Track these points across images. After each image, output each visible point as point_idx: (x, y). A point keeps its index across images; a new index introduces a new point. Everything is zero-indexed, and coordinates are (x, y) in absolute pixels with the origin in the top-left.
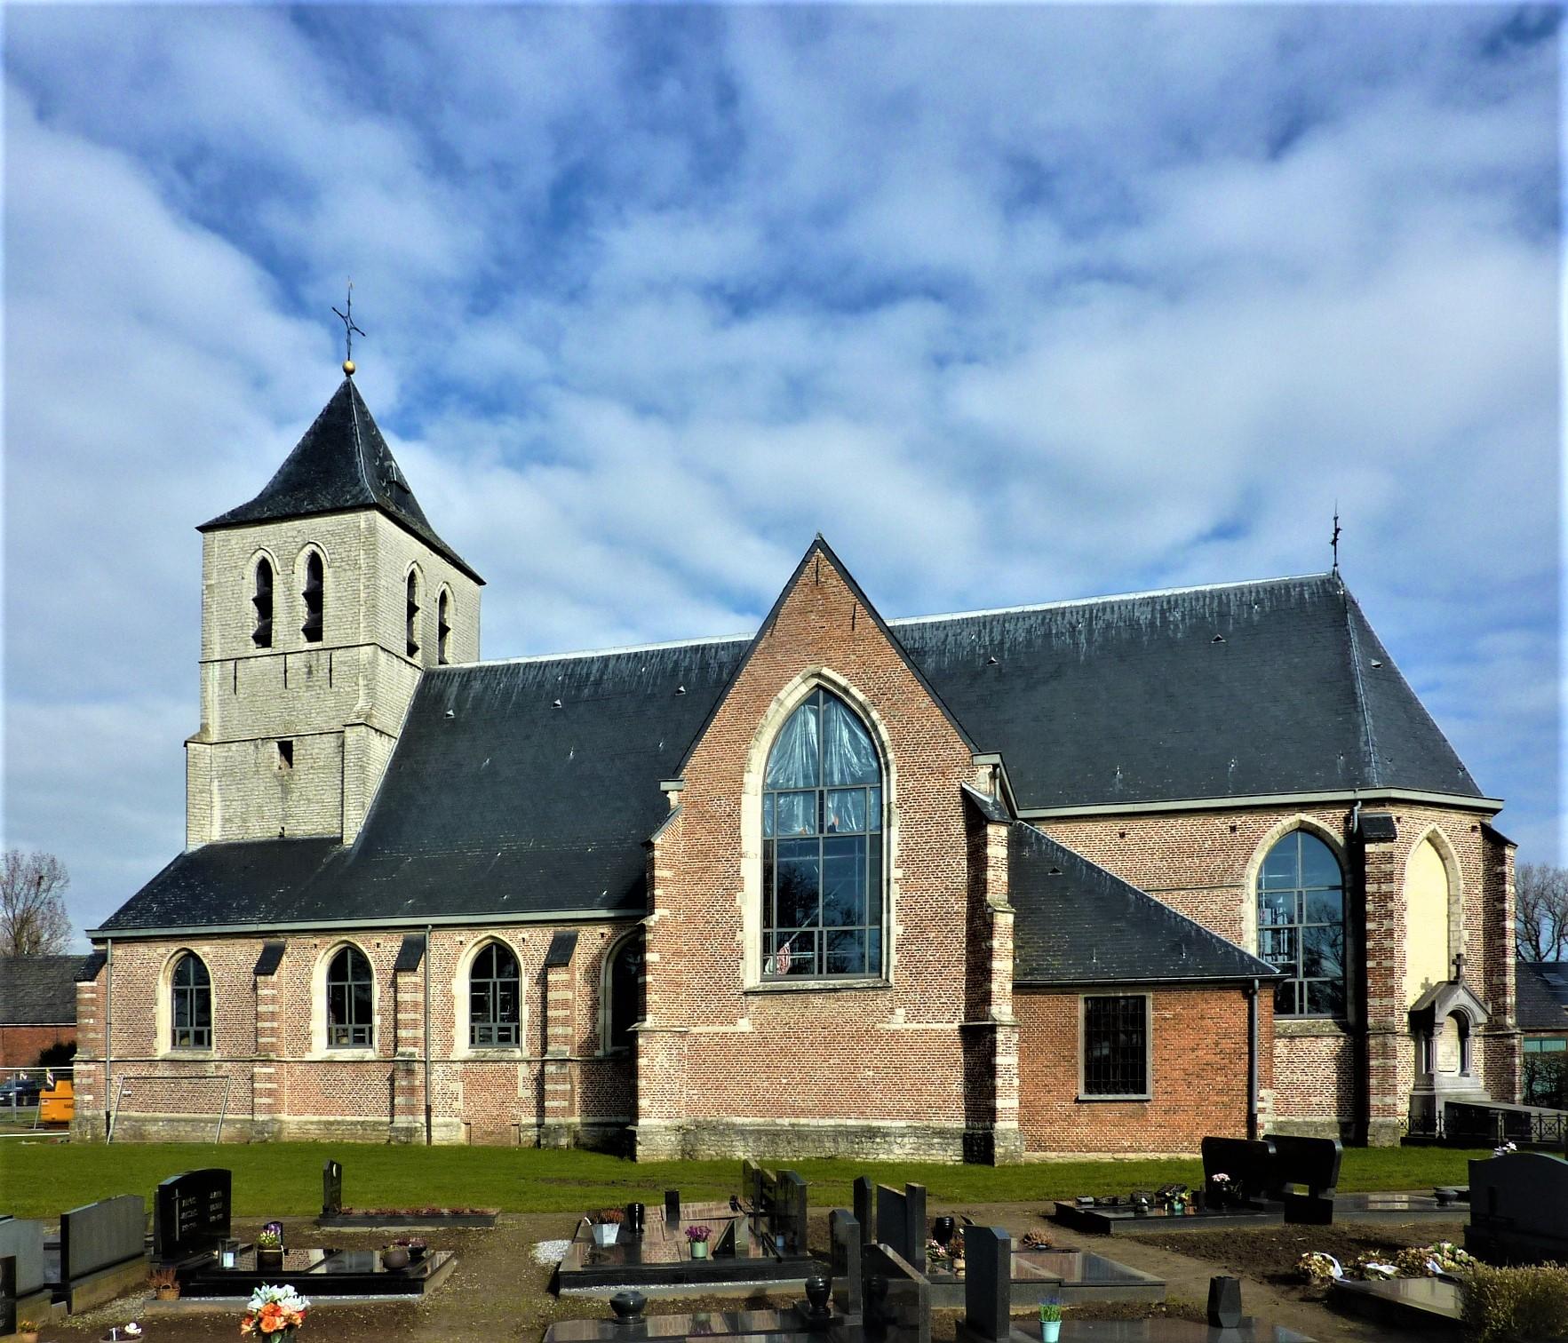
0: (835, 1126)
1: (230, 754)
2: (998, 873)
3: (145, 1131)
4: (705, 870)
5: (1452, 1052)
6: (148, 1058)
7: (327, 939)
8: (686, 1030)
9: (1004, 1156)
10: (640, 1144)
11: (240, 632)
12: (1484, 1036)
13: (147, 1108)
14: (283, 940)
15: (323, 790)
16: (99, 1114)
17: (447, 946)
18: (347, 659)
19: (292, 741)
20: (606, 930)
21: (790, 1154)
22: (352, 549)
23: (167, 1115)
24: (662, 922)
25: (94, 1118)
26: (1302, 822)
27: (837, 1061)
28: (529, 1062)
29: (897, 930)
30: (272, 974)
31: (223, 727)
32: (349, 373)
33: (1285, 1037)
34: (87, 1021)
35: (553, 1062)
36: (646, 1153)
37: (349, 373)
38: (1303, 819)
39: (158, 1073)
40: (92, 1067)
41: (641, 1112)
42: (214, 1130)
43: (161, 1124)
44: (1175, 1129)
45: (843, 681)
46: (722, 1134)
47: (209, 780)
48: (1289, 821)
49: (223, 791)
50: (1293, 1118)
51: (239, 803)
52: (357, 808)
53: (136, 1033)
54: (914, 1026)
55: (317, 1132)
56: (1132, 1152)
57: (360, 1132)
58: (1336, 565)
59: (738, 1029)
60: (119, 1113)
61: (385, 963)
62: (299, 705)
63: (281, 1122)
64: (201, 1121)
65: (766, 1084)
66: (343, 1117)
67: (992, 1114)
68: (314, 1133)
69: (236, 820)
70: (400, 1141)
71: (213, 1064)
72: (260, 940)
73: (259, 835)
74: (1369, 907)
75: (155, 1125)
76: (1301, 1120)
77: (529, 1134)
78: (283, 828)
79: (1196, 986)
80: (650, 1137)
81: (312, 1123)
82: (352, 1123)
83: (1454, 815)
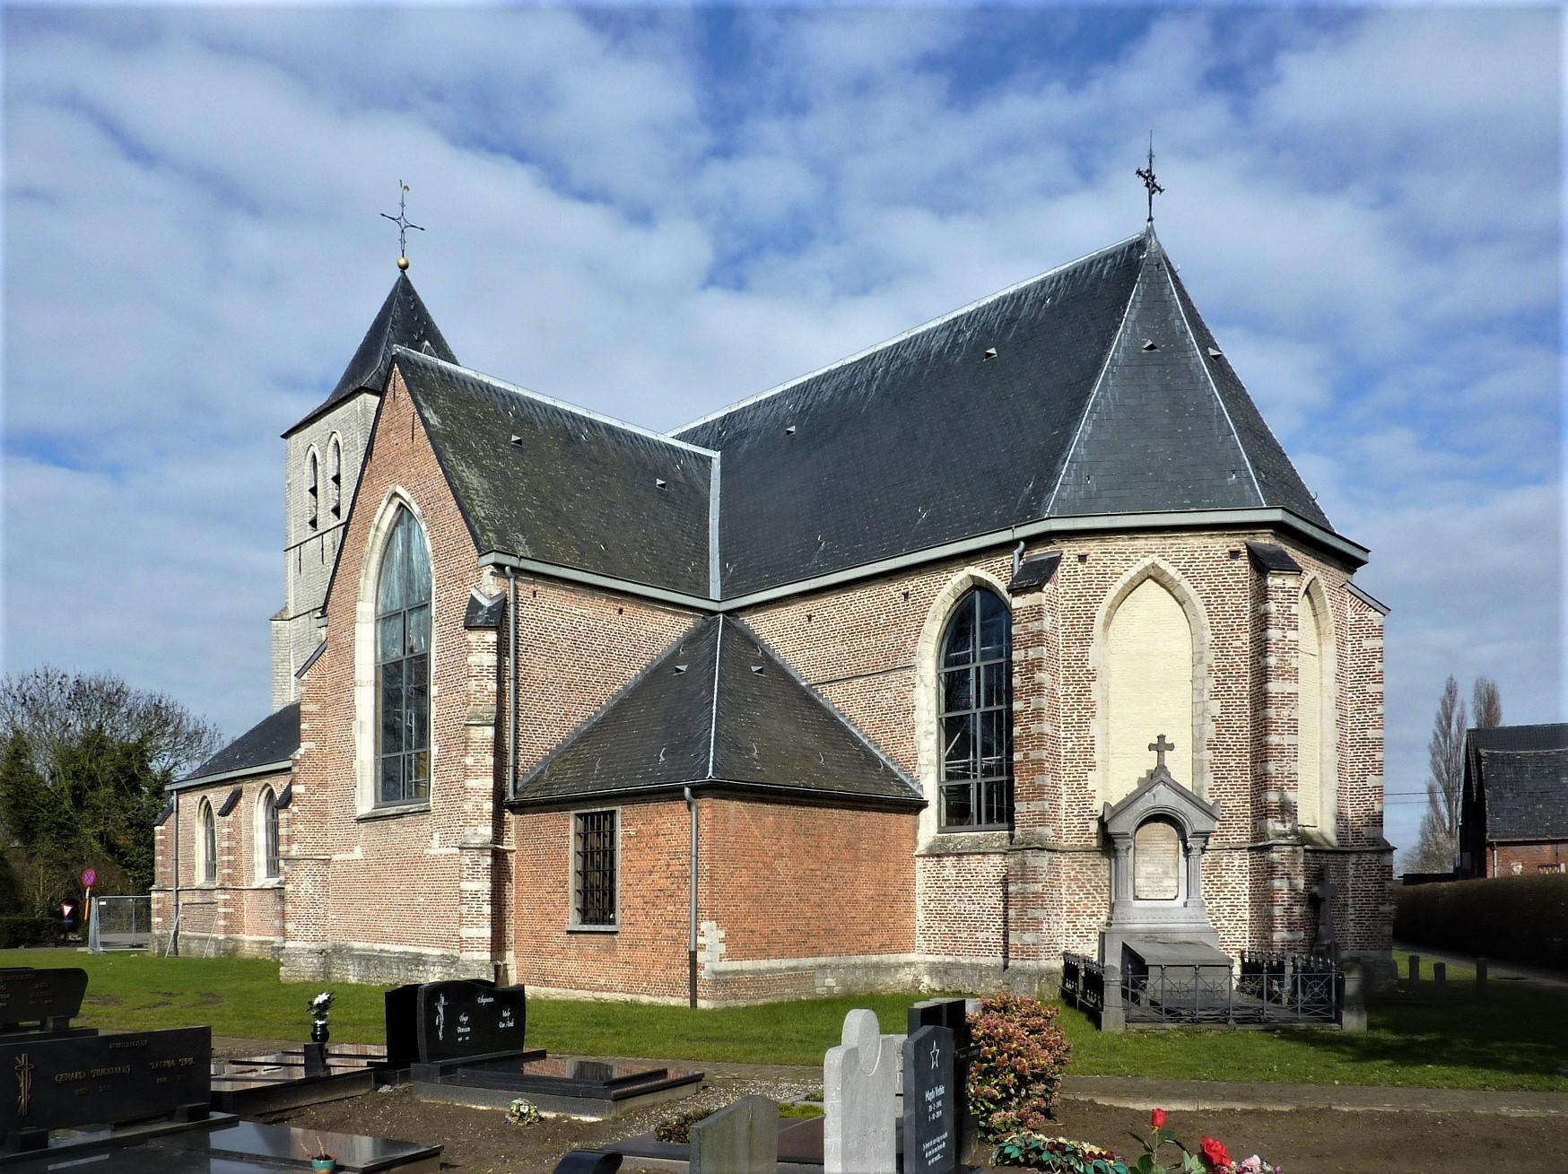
0: (401, 953)
2: (482, 683)
5: (1167, 874)
8: (328, 857)
10: (283, 965)
12: (1250, 849)
16: (169, 934)
24: (308, 755)
25: (163, 937)
26: (973, 577)
30: (1039, 588)
32: (404, 268)
33: (953, 855)
36: (289, 974)
37: (404, 268)
38: (972, 573)
40: (161, 895)
44: (637, 965)
48: (958, 579)
50: (960, 958)
54: (445, 851)
56: (607, 991)
58: (1150, 219)
60: (183, 933)
63: (236, 941)
74: (1016, 681)
76: (968, 961)
79: (653, 797)
80: (293, 959)
83: (1191, 540)
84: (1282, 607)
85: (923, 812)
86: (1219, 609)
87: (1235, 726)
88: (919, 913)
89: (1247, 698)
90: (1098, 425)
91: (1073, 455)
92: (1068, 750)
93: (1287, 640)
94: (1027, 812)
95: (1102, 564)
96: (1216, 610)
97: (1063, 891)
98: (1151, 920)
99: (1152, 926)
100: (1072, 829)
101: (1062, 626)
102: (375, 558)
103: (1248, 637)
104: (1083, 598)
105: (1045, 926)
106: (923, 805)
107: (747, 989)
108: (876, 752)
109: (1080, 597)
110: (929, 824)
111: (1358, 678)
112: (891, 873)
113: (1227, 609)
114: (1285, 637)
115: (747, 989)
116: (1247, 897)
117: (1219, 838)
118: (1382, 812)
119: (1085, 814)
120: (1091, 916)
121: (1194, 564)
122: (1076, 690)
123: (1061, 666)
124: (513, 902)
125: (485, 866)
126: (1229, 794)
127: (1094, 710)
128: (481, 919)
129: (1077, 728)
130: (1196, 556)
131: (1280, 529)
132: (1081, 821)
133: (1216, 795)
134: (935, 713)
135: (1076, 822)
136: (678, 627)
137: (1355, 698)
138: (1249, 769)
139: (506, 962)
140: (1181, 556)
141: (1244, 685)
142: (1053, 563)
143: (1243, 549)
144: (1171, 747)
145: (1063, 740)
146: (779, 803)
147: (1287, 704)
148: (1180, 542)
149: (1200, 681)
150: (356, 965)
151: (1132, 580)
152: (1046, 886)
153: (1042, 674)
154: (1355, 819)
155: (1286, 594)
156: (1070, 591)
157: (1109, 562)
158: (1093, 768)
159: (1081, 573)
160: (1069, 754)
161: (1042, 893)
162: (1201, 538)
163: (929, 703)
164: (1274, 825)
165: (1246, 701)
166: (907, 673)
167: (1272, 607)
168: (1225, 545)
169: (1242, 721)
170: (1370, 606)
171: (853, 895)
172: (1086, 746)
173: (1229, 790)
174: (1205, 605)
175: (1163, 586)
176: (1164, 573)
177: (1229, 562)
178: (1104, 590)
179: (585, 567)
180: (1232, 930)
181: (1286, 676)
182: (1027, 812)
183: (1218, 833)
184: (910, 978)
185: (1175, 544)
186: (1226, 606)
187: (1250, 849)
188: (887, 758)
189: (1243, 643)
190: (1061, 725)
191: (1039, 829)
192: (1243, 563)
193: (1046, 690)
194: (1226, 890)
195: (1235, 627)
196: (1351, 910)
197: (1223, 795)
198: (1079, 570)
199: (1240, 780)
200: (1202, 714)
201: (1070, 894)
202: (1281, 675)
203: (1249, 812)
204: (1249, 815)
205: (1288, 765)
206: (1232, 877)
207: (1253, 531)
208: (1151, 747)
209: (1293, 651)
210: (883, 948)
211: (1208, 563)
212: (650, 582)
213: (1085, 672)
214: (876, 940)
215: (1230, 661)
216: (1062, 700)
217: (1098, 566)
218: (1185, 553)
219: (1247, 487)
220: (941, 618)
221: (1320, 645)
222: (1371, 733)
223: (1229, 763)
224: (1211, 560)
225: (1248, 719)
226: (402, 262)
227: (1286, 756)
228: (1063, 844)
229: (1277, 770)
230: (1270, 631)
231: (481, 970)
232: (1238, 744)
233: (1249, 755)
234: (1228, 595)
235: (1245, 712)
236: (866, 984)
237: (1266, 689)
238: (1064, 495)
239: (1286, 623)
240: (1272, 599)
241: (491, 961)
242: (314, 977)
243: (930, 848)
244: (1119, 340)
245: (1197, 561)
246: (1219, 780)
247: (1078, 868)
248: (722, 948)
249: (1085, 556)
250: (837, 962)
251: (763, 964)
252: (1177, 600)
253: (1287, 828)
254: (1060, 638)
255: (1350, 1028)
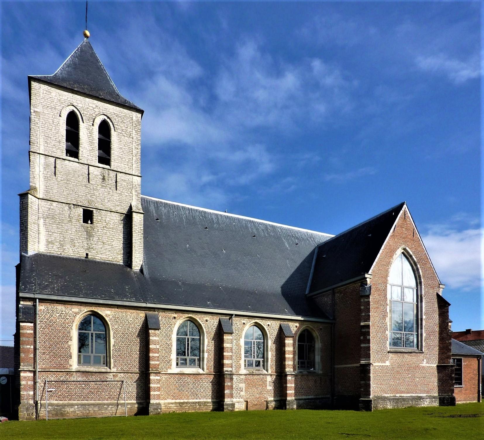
1: (52, 207)
3: (65, 411)
4: (377, 308)
6: (66, 370)
7: (181, 315)
11: (58, 144)
13: (64, 398)
14: (157, 313)
15: (112, 239)
17: (238, 324)
18: (125, 179)
19: (93, 211)
20: (298, 325)
21: (401, 406)
22: (128, 127)
23: (79, 402)
27: (410, 376)
28: (271, 375)
29: (424, 335)
31: (47, 192)
34: (28, 347)
35: (290, 375)
39: (72, 379)
42: (113, 409)
43: (76, 407)
45: (411, 253)
46: (384, 400)
47: (37, 218)
49: (47, 226)
51: (59, 235)
52: (140, 253)
53: (55, 355)
54: (428, 365)
55: (175, 407)
57: (198, 407)
59: (386, 364)
61: (210, 329)
62: (97, 194)
64: (104, 404)
65: (393, 383)
66: (188, 400)
67: (286, 395)
68: (174, 408)
69: (57, 244)
70: (229, 410)
71: (111, 374)
72: (144, 312)
73: (72, 254)
75: (72, 408)
77: (272, 404)
78: (87, 254)
81: (172, 403)
82: (193, 403)
150: (391, 402)
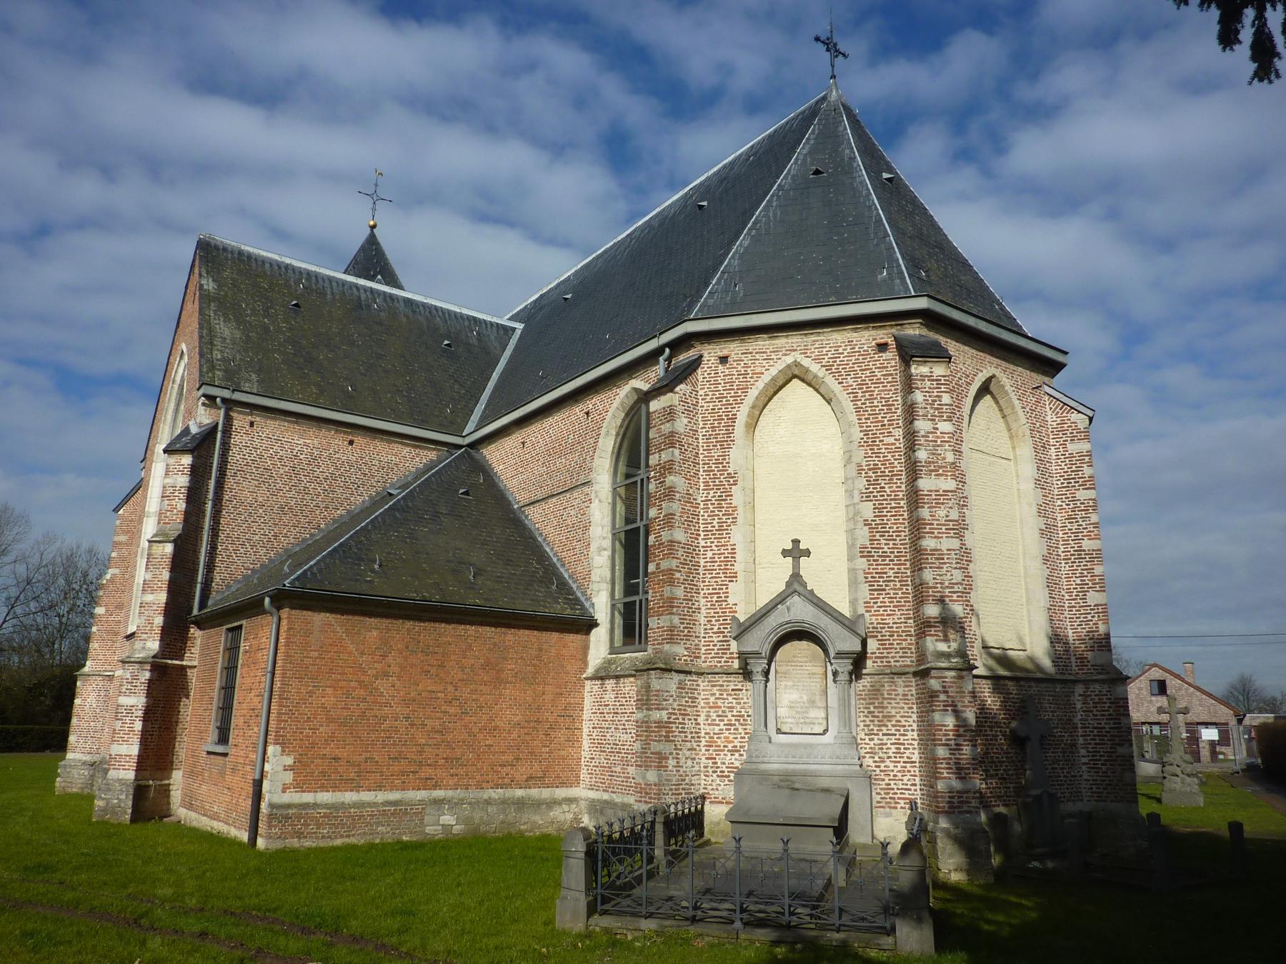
5: (813, 702)
9: (105, 810)
24: (112, 580)
26: (636, 390)
36: (63, 784)
37: (373, 227)
41: (69, 747)
80: (68, 770)
84: (930, 396)
85: (594, 631)
86: (868, 405)
87: (891, 530)
88: (585, 743)
89: (903, 499)
90: (755, 240)
91: (726, 266)
92: (708, 560)
93: (938, 432)
94: (658, 628)
95: (742, 365)
96: (864, 406)
97: (701, 720)
98: (791, 760)
99: (791, 767)
100: (711, 647)
101: (702, 428)
102: (172, 405)
103: (901, 433)
104: (724, 400)
105: (671, 762)
106: (592, 624)
107: (319, 826)
108: (562, 570)
109: (720, 399)
110: (599, 645)
111: (1065, 485)
112: (548, 697)
113: (876, 404)
114: (937, 429)
115: (319, 826)
116: (915, 733)
117: (879, 660)
118: (1109, 635)
119: (726, 631)
120: (733, 752)
121: (838, 360)
122: (717, 495)
123: (701, 470)
124: (188, 718)
125: (143, 681)
126: (888, 609)
127: (735, 516)
128: (131, 736)
129: (717, 536)
130: (841, 350)
131: (928, 317)
132: (721, 638)
133: (873, 609)
134: (609, 528)
135: (715, 640)
136: (417, 459)
137: (1064, 506)
138: (909, 579)
139: (172, 781)
140: (824, 353)
141: (899, 485)
142: (696, 363)
143: (890, 341)
144: (807, 553)
145: (702, 550)
146: (387, 617)
147: (943, 504)
148: (822, 338)
149: (850, 481)
151: (774, 379)
152: (675, 714)
153: (672, 478)
154: (1077, 642)
155: (935, 383)
156: (710, 393)
157: (750, 362)
158: (734, 579)
159: (722, 375)
160: (709, 564)
161: (666, 722)
162: (845, 333)
163: (604, 517)
164: (935, 645)
165: (902, 502)
166: (586, 489)
167: (918, 397)
168: (871, 338)
169: (899, 524)
170: (1072, 408)
171: (491, 720)
172: (726, 555)
173: (888, 604)
174: (852, 401)
175: (809, 385)
176: (807, 370)
177: (876, 356)
178: (745, 390)
179: (319, 403)
180: (900, 774)
181: (941, 471)
182: (658, 628)
183: (877, 655)
184: (570, 816)
185: (817, 341)
186: (875, 401)
187: (915, 674)
188: (569, 576)
189: (896, 440)
190: (701, 533)
191: (667, 647)
192: (891, 356)
193: (678, 495)
194: (889, 724)
195: (886, 422)
196: (1083, 752)
197: (881, 609)
198: (720, 371)
199: (900, 592)
200: (853, 518)
201: (709, 724)
202: (933, 471)
203: (912, 630)
204: (913, 633)
205: (949, 574)
206: (895, 708)
207: (900, 322)
208: (785, 553)
209: (947, 444)
210: (530, 781)
211: (854, 358)
212: (393, 418)
213: (726, 475)
214: (522, 771)
215: (882, 459)
216: (702, 506)
217: (739, 367)
218: (828, 349)
219: (898, 281)
220: (614, 433)
221: (1014, 448)
222: (1087, 544)
223: (886, 573)
224: (857, 354)
225: (906, 522)
226: (372, 223)
227: (945, 563)
228: (702, 664)
229: (934, 579)
230: (916, 423)
231: (121, 790)
232: (896, 551)
233: (908, 563)
234: (877, 389)
235: (903, 515)
236: (503, 822)
237: (917, 487)
238: (711, 302)
239: (936, 413)
240: (918, 388)
241: (135, 780)
242: (82, 789)
243: (597, 671)
244: (789, 170)
245: (842, 356)
246: (876, 593)
247: (718, 693)
248: (289, 777)
249: (727, 357)
250: (462, 795)
251: (349, 797)
252: (824, 398)
253: (952, 649)
254: (700, 441)
255: (908, 948)
